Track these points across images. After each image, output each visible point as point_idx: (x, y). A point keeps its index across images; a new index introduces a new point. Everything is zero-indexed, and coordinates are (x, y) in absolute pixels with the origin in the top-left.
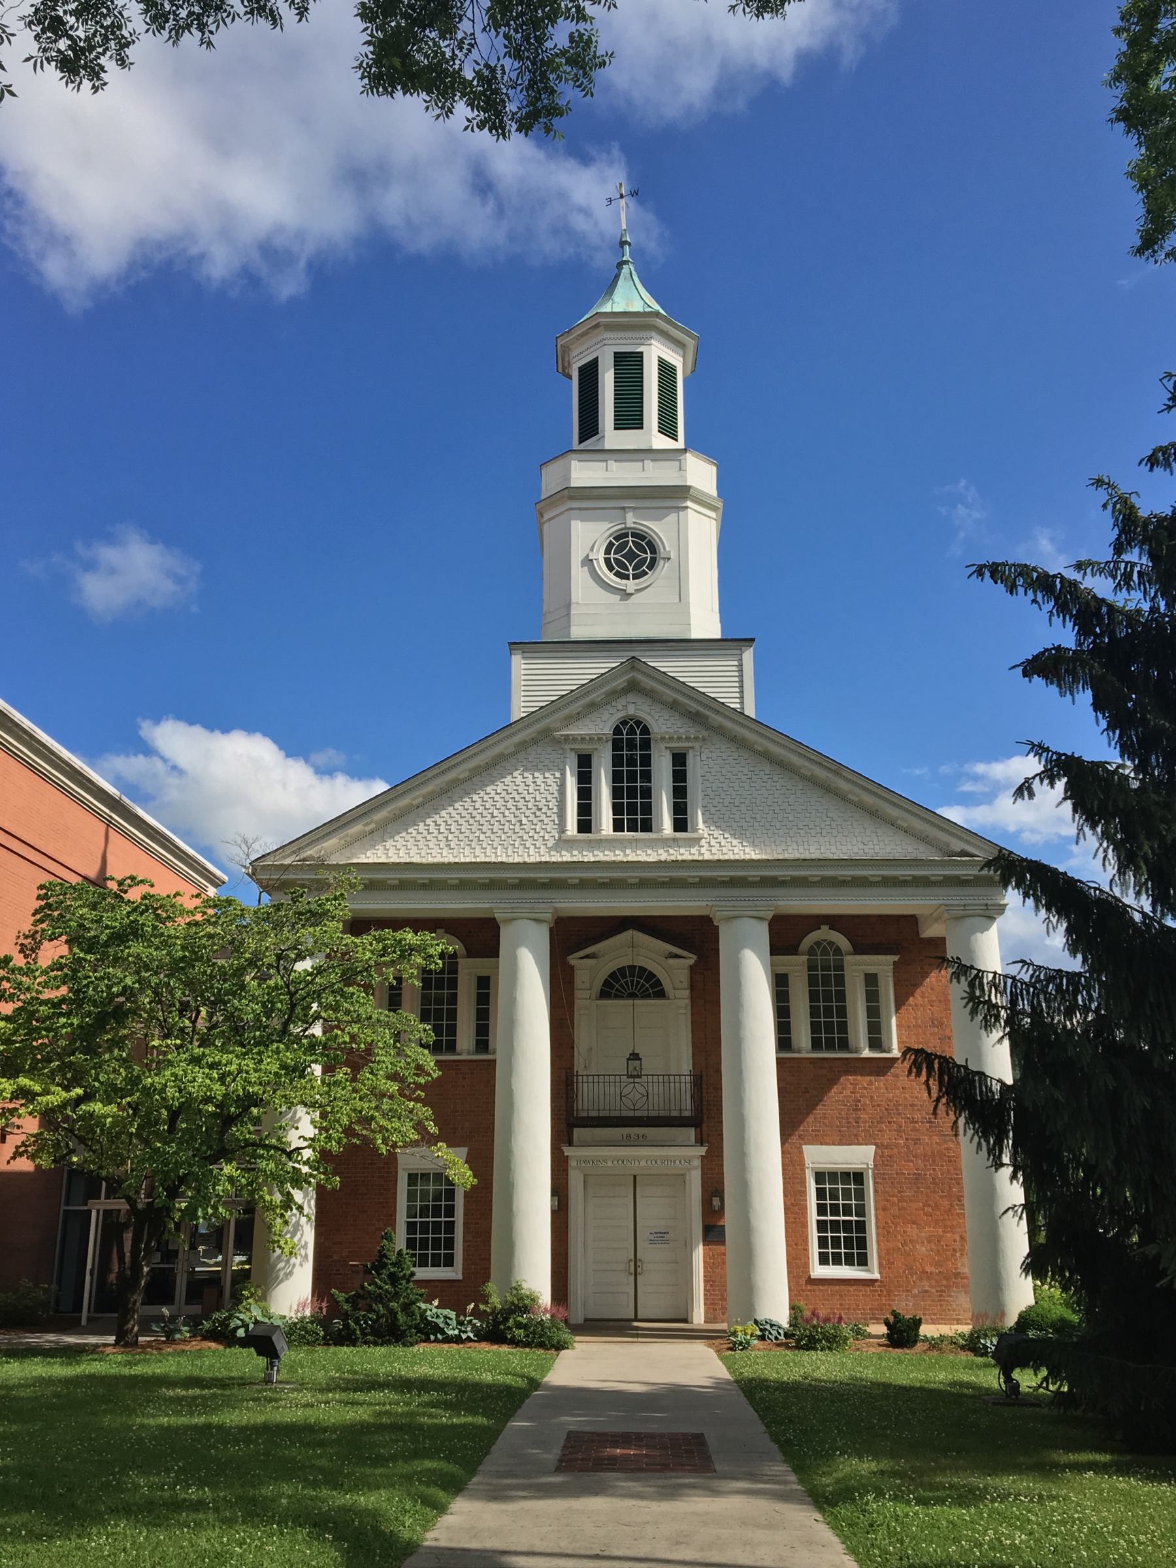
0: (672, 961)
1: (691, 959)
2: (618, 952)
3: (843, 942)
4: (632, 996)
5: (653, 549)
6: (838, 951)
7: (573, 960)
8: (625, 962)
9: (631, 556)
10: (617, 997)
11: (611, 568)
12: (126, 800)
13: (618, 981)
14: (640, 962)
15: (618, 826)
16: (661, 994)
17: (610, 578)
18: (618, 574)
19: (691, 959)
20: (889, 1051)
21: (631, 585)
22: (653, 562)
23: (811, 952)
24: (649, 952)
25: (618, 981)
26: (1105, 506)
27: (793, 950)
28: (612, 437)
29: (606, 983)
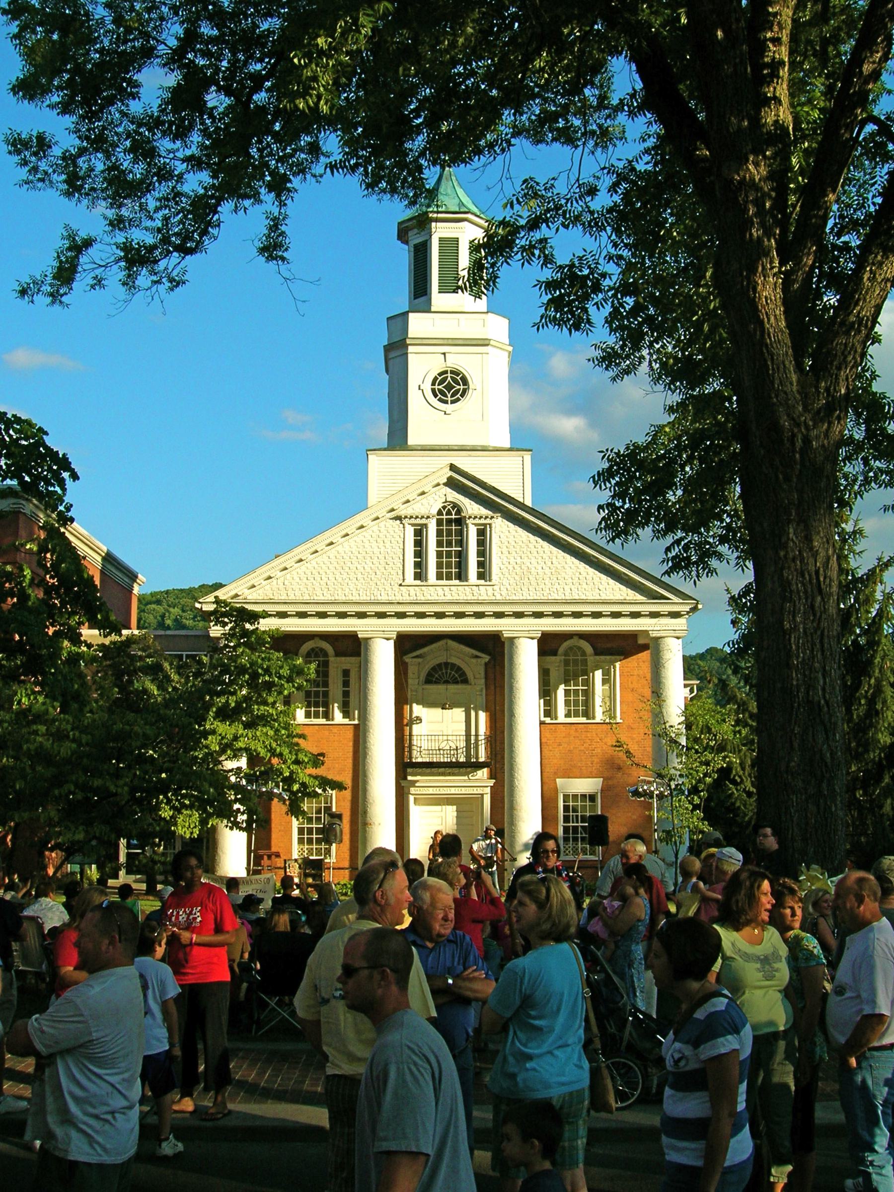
0: (474, 660)
1: (486, 658)
2: (434, 655)
3: (589, 649)
4: (446, 682)
5: (465, 381)
6: (584, 654)
7: (407, 659)
8: (441, 659)
9: (449, 387)
10: (436, 683)
11: (435, 396)
12: (93, 539)
13: (446, 668)
14: (453, 660)
15: (439, 577)
16: (465, 681)
17: (434, 401)
18: (440, 400)
19: (486, 658)
20: (594, 718)
21: (449, 408)
22: (464, 391)
23: (566, 654)
24: (461, 655)
25: (446, 668)
26: (600, 507)
27: (554, 653)
28: (439, 300)
29: (429, 675)
